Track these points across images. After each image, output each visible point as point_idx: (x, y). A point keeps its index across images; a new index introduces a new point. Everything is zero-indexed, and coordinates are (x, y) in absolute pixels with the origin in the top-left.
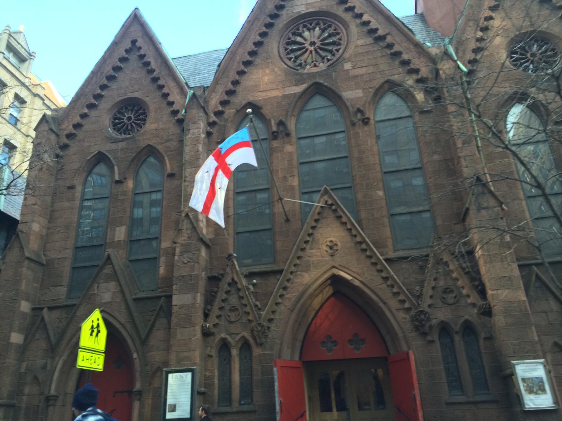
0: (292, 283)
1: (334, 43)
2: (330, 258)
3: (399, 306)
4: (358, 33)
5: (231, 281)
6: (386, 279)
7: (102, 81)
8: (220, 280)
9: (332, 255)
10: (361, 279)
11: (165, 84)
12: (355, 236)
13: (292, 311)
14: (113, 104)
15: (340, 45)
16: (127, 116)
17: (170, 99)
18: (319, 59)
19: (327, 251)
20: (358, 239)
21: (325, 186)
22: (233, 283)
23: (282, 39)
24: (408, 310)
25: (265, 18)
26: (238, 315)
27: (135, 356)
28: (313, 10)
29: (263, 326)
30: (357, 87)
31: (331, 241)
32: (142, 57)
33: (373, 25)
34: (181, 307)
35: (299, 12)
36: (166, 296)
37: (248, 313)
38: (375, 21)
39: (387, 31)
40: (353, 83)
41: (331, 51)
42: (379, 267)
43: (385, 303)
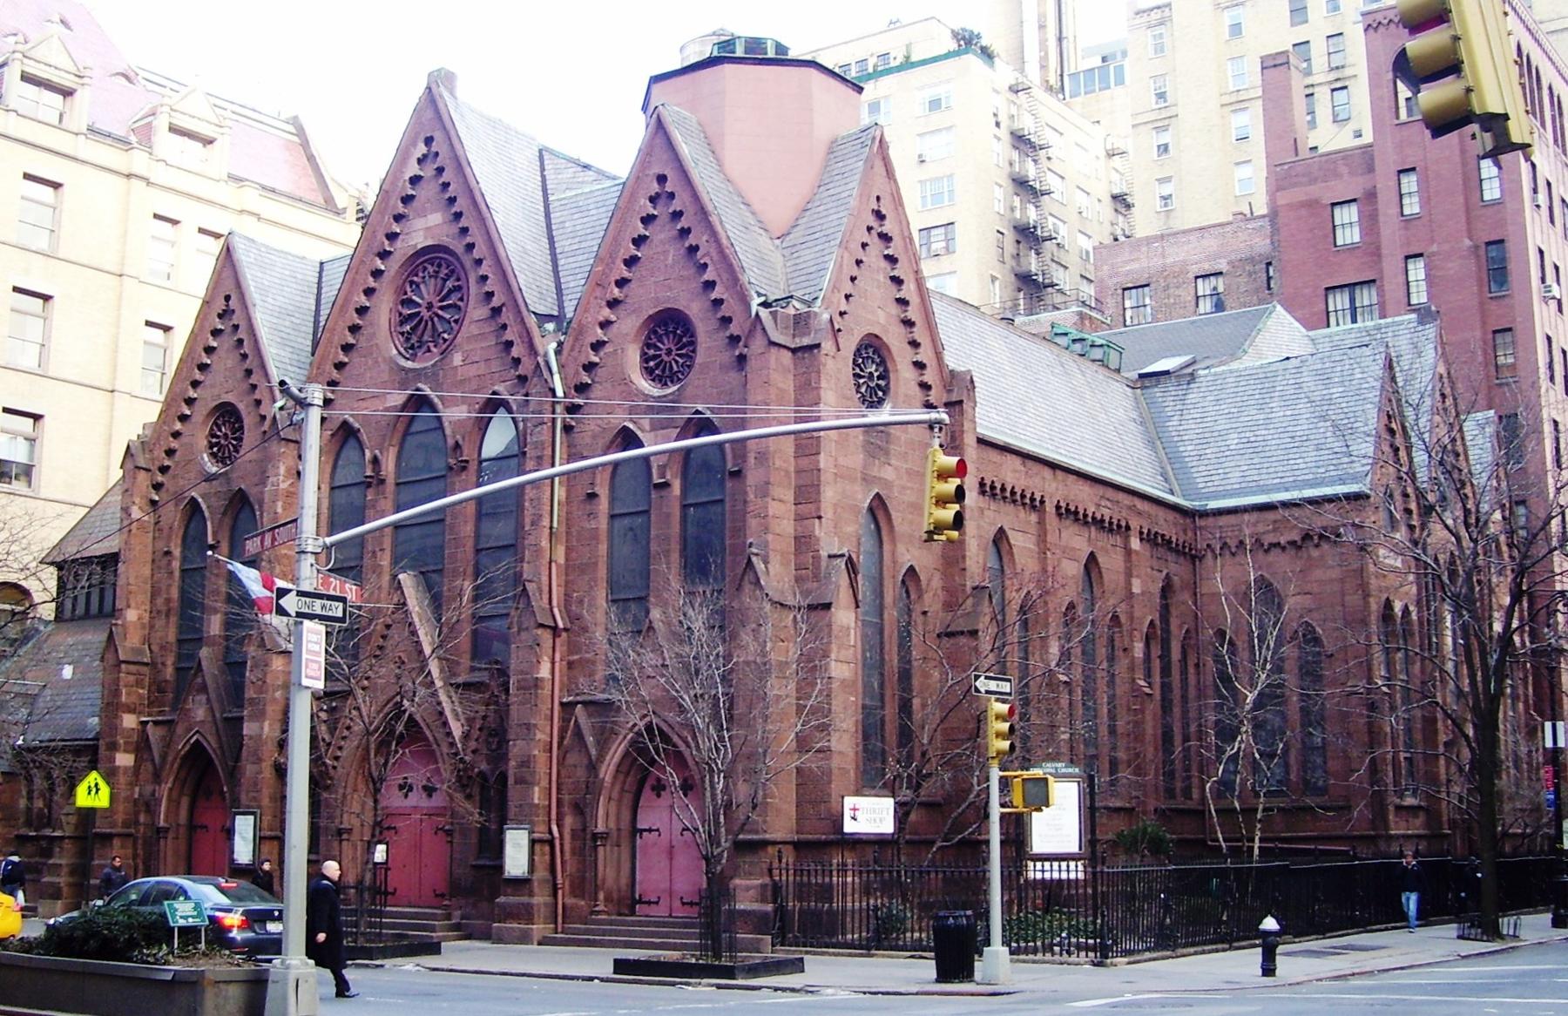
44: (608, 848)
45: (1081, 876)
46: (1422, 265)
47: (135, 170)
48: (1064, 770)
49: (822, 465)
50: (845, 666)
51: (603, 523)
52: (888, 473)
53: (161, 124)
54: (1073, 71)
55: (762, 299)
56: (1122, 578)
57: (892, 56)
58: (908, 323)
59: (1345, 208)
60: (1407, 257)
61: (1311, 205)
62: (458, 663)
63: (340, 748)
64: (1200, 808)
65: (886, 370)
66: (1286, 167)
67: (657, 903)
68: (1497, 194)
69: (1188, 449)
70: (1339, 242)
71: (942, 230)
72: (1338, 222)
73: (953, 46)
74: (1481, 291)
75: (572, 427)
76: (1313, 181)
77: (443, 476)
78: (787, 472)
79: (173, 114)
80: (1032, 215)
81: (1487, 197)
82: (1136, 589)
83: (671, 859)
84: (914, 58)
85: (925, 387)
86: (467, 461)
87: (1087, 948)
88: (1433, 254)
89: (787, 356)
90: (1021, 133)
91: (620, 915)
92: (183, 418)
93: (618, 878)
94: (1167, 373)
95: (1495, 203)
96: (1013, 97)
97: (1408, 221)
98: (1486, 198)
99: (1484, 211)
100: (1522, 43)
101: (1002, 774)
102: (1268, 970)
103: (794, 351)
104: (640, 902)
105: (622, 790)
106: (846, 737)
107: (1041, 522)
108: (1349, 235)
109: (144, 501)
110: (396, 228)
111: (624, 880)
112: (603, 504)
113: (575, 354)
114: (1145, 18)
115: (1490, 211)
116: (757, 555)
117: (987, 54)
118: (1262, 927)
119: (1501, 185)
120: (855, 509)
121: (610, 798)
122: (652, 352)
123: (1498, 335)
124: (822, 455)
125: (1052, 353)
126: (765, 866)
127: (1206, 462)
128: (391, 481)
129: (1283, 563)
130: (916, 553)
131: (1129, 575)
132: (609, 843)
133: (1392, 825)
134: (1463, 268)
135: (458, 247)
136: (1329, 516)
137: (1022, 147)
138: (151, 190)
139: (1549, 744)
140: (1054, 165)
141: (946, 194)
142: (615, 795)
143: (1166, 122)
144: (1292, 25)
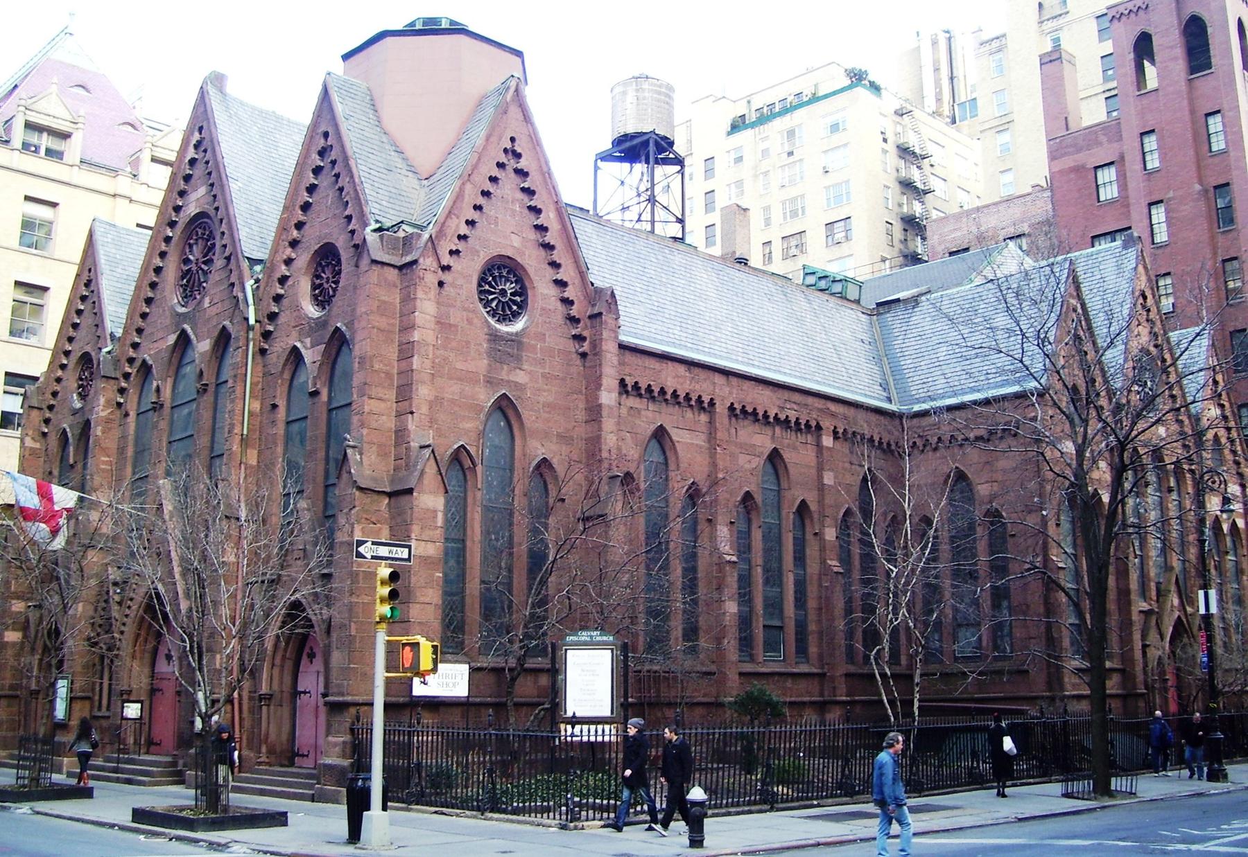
44: (272, 707)
45: (613, 739)
46: (1163, 209)
47: (118, 192)
48: (599, 638)
49: (415, 367)
50: (430, 545)
51: (280, 429)
52: (520, 377)
53: (146, 156)
54: (963, 99)
55: (378, 225)
56: (814, 471)
57: (804, 94)
58: (548, 247)
59: (1106, 170)
60: (1150, 205)
61: (1078, 169)
62: (876, 580)
63: (124, 624)
64: (908, 672)
65: (523, 288)
66: (1058, 140)
68: (1222, 146)
69: (907, 363)
70: (1102, 198)
71: (842, 223)
72: (1100, 182)
73: (847, 82)
74: (1211, 229)
75: (266, 350)
76: (1079, 150)
77: (195, 399)
78: (388, 374)
79: (154, 149)
80: (917, 209)
81: (1215, 148)
82: (828, 479)
83: (317, 718)
84: (821, 94)
85: (567, 302)
86: (207, 385)
87: (602, 809)
88: (1170, 199)
89: (392, 274)
90: (906, 146)
91: (282, 766)
92: (63, 367)
93: (279, 735)
94: (898, 300)
95: (1223, 153)
96: (898, 119)
97: (1149, 174)
98: (1213, 149)
99: (1210, 160)
100: (1244, 20)
101: (387, 638)
102: (696, 841)
103: (400, 268)
104: (298, 755)
105: (284, 657)
106: (431, 609)
107: (711, 422)
108: (1109, 192)
109: (36, 433)
111: (284, 737)
112: (281, 413)
113: (268, 289)
114: (988, 47)
115: (1216, 160)
116: (353, 447)
117: (875, 87)
118: (689, 797)
119: (1226, 137)
120: (478, 408)
121: (273, 665)
122: (318, 282)
123: (1226, 264)
124: (416, 357)
125: (776, 284)
126: (348, 725)
127: (920, 373)
128: (168, 405)
129: (972, 459)
130: (554, 447)
131: (820, 469)
132: (273, 701)
133: (1068, 686)
134: (1194, 209)
135: (212, 213)
136: (1012, 414)
137: (908, 157)
138: (133, 205)
139: (1202, 611)
140: (937, 170)
141: (845, 196)
142: (278, 661)
143: (1006, 126)
144: (1100, 41)
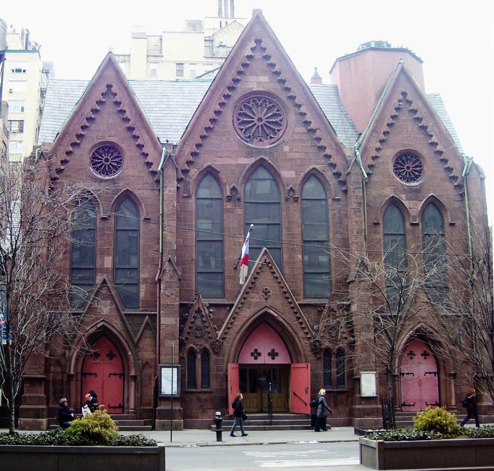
0: (239, 315)
1: (276, 123)
2: (264, 300)
3: (304, 336)
4: (296, 121)
5: (197, 310)
6: (298, 318)
7: (83, 122)
8: (190, 308)
9: (266, 299)
10: (283, 317)
11: (140, 136)
12: (283, 288)
13: (238, 333)
14: (94, 145)
15: (281, 126)
16: (105, 158)
17: (145, 150)
18: (264, 135)
19: (263, 296)
20: (285, 290)
21: (265, 248)
22: (199, 311)
23: (236, 109)
24: (309, 338)
25: (224, 89)
26: (202, 333)
27: (130, 353)
28: (263, 90)
29: (219, 342)
30: (292, 168)
31: (266, 289)
32: (118, 103)
33: (308, 118)
34: (167, 326)
35: (252, 89)
36: (150, 315)
37: (209, 333)
38: (310, 115)
39: (318, 126)
40: (289, 165)
41: (273, 130)
42: (295, 310)
43: (296, 333)
67: (414, 405)
102: (219, 438)
110: (239, 77)
